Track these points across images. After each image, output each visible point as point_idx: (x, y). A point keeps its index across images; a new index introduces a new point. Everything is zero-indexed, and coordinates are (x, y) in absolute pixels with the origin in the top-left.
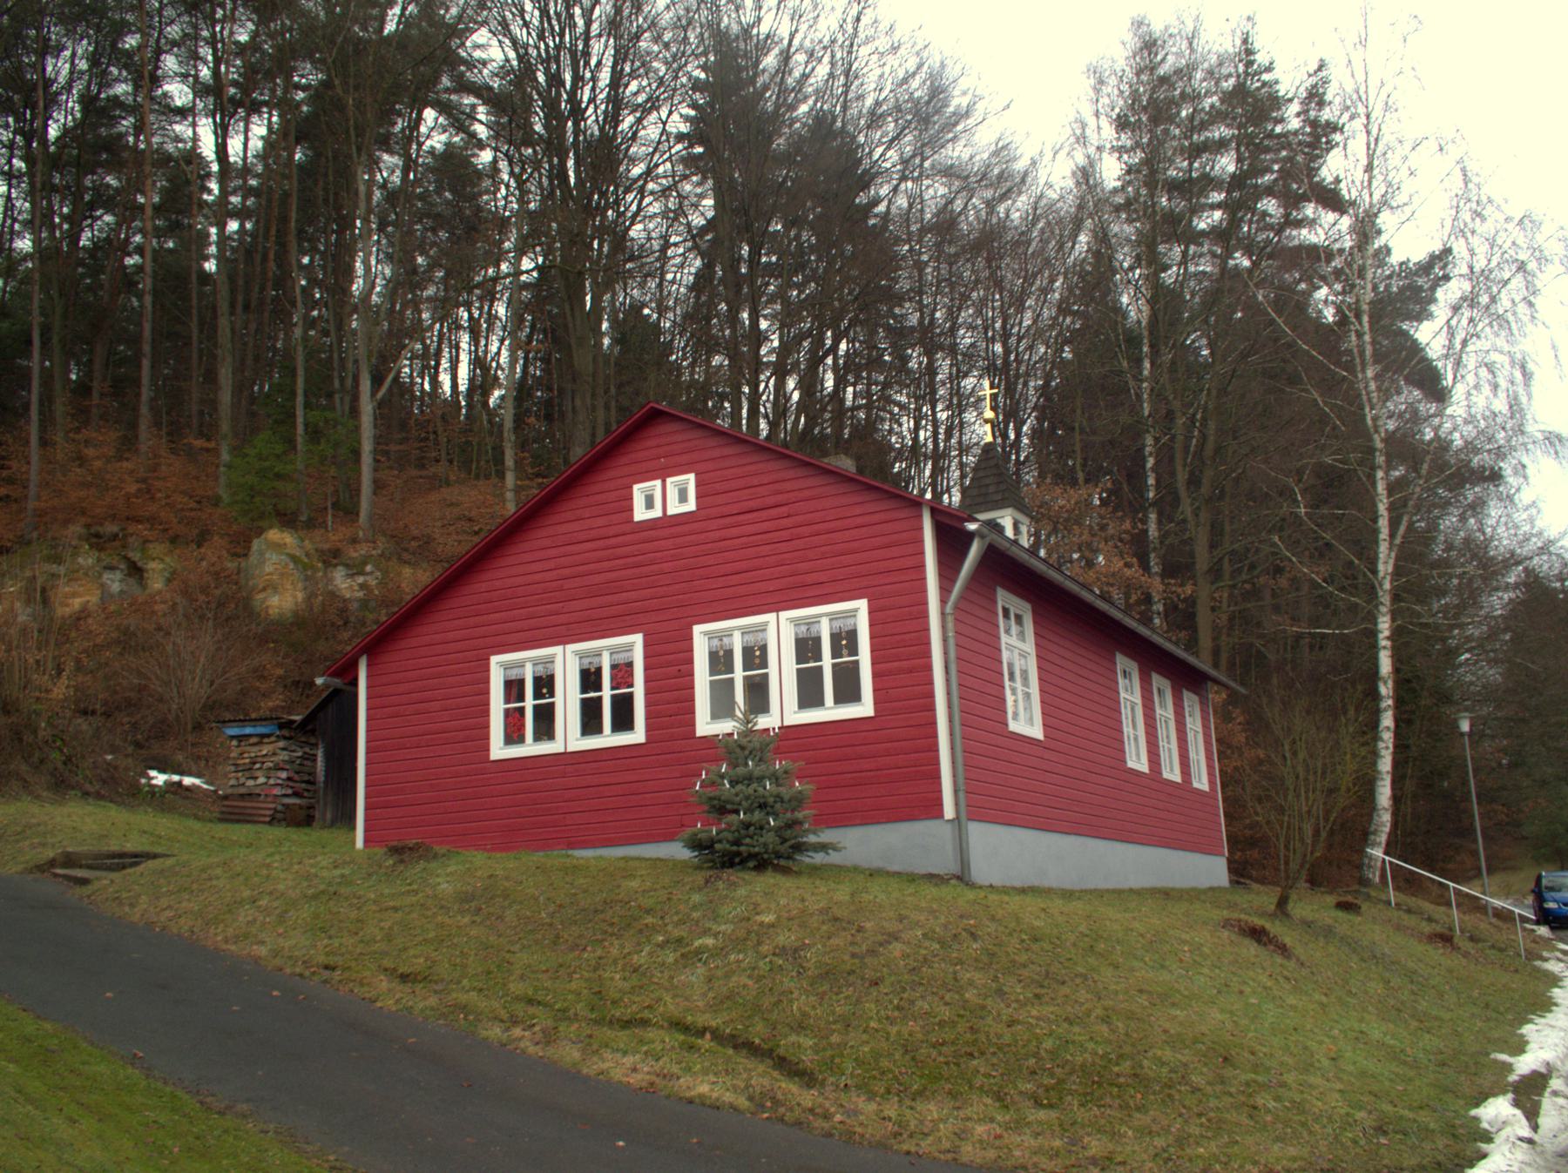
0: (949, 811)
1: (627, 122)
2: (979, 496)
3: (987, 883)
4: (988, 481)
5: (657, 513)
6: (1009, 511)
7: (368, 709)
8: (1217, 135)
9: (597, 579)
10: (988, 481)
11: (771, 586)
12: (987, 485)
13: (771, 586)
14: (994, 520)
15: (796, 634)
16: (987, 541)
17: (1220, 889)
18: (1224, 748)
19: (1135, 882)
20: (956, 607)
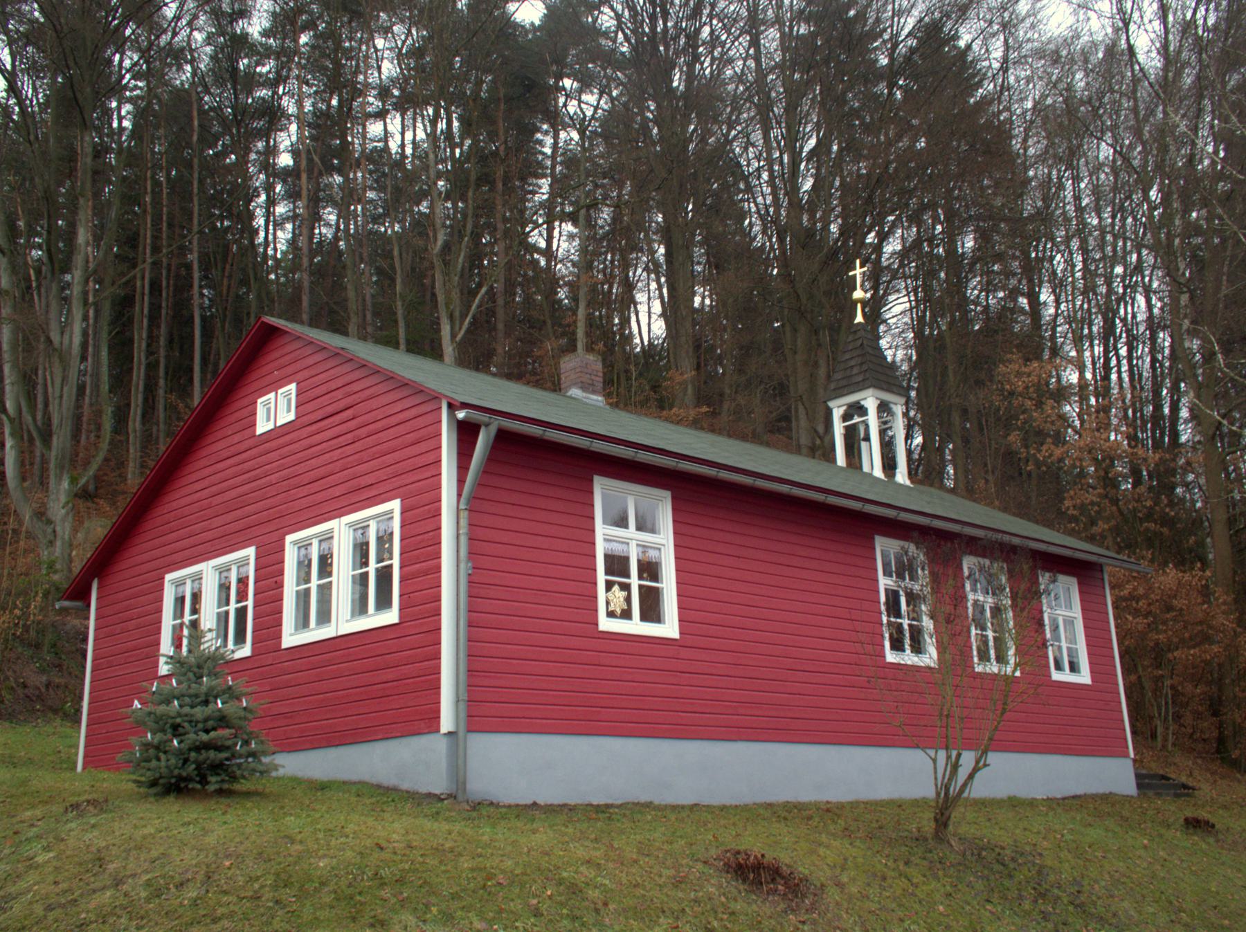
0: (447, 722)
1: (752, 51)
2: (844, 378)
3: (530, 802)
4: (852, 363)
5: (270, 426)
6: (870, 392)
7: (437, 656)
8: (389, 69)
9: (233, 493)
10: (852, 363)
11: (337, 491)
12: (852, 367)
13: (337, 491)
14: (858, 402)
15: (355, 539)
16: (493, 430)
17: (1132, 797)
18: (934, 625)
19: (1039, 792)
20: (469, 501)
